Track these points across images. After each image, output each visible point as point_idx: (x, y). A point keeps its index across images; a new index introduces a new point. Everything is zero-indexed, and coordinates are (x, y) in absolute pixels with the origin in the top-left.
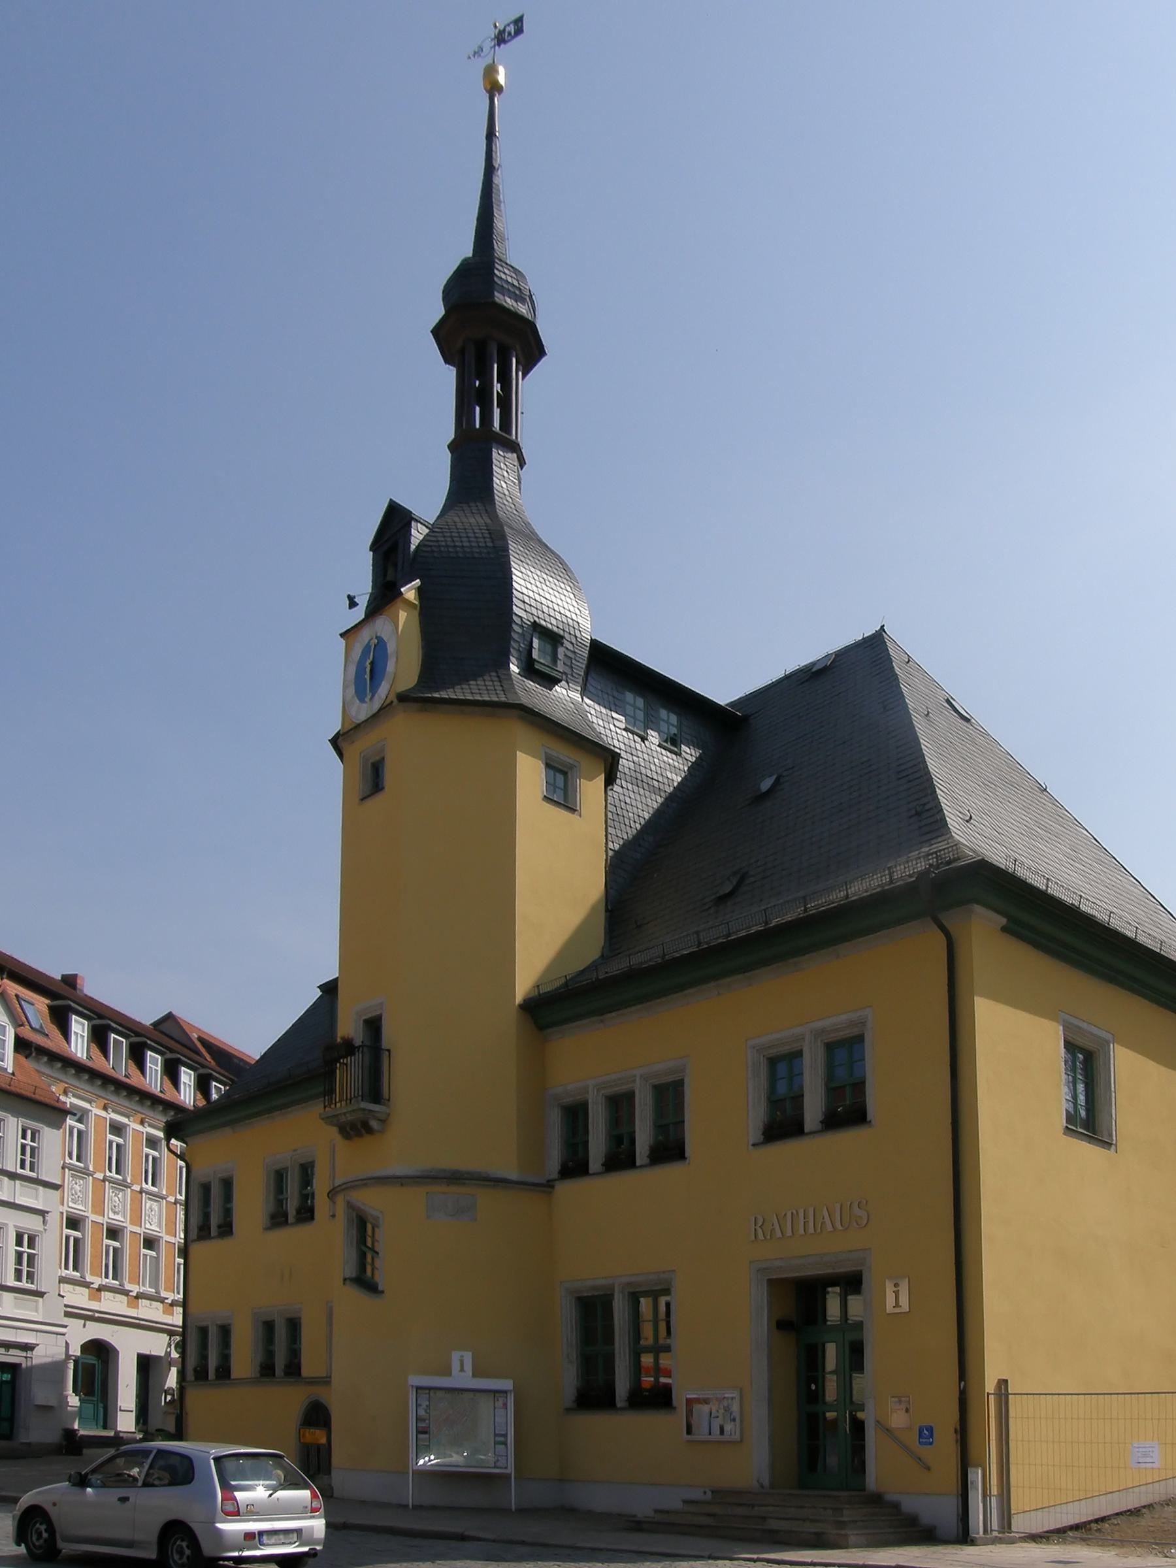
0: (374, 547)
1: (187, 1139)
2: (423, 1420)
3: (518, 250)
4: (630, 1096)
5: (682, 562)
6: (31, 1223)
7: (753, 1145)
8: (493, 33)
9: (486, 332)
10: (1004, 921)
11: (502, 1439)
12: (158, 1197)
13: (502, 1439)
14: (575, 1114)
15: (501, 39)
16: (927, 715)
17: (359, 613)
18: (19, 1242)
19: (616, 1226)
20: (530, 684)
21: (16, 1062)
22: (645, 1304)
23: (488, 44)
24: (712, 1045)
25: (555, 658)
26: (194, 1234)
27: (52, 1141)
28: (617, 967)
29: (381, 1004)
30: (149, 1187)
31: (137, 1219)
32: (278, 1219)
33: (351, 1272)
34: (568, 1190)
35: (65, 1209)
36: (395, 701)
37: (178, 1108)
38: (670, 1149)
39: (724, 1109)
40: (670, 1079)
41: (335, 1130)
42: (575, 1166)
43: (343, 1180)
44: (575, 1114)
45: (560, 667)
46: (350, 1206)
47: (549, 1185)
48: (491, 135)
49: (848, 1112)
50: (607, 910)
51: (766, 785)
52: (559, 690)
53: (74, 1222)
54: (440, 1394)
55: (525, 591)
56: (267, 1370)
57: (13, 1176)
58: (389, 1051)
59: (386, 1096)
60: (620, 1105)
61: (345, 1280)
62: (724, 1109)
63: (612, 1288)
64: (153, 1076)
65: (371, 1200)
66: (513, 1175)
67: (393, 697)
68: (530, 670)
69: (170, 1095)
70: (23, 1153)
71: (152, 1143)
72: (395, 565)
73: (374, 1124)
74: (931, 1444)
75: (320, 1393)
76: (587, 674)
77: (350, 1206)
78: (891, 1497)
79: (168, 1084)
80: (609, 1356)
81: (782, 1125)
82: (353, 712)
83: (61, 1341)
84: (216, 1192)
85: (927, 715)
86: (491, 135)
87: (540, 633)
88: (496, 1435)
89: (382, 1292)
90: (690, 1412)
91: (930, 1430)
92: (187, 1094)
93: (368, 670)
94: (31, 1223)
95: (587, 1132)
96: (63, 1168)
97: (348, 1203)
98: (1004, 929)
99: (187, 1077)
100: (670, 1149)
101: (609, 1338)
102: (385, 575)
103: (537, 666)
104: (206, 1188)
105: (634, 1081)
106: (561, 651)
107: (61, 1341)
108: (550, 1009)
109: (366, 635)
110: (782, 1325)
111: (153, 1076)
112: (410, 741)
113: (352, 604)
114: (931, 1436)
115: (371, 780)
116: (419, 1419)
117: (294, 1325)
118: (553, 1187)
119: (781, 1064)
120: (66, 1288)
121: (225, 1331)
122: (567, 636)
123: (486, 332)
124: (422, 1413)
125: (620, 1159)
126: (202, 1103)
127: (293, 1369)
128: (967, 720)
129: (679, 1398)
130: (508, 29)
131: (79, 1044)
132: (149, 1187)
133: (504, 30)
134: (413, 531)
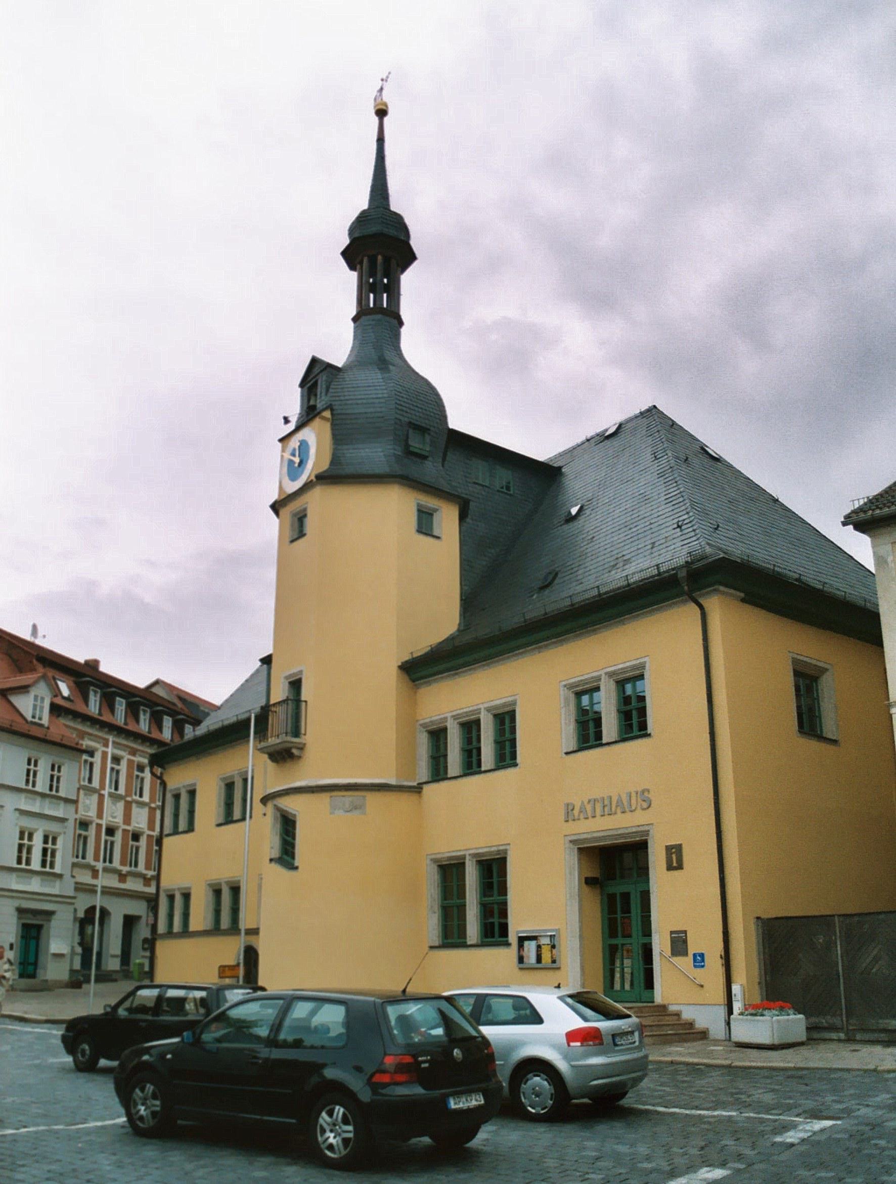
0: (302, 385)
4: (477, 722)
6: (54, 827)
9: (379, 248)
10: (742, 595)
12: (142, 804)
14: (438, 735)
16: (686, 459)
17: (291, 426)
18: (46, 841)
19: (471, 814)
21: (50, 721)
24: (536, 686)
27: (70, 777)
28: (468, 638)
29: (301, 672)
30: (137, 798)
31: (127, 819)
32: (228, 819)
33: (276, 853)
35: (78, 816)
37: (161, 743)
38: (507, 756)
39: (545, 725)
40: (507, 709)
41: (266, 756)
42: (439, 773)
44: (438, 735)
46: (277, 808)
47: (417, 789)
48: (381, 140)
49: (634, 720)
50: (461, 600)
51: (574, 511)
52: (428, 464)
53: (84, 824)
57: (43, 795)
58: (306, 702)
59: (303, 731)
61: (271, 860)
62: (545, 725)
63: (464, 857)
64: (144, 725)
65: (290, 804)
66: (393, 781)
67: (313, 477)
69: (155, 735)
70: (52, 780)
71: (141, 768)
72: (316, 395)
73: (295, 751)
74: (703, 966)
75: (252, 940)
76: (447, 447)
77: (277, 808)
78: (673, 1008)
79: (154, 726)
81: (589, 733)
82: (284, 485)
83: (71, 908)
85: (686, 459)
87: (414, 429)
89: (297, 868)
91: (702, 955)
92: (167, 734)
94: (54, 827)
95: (446, 749)
96: (79, 789)
98: (743, 600)
99: (168, 722)
101: (462, 894)
102: (309, 400)
105: (480, 713)
107: (71, 908)
108: (419, 670)
109: (294, 443)
110: (589, 882)
111: (144, 725)
112: (320, 502)
113: (286, 420)
114: (703, 961)
115: (298, 528)
117: (235, 890)
118: (422, 788)
119: (584, 690)
120: (76, 871)
121: (187, 896)
122: (432, 428)
125: (471, 764)
126: (177, 741)
127: (234, 929)
131: (94, 706)
132: (137, 798)
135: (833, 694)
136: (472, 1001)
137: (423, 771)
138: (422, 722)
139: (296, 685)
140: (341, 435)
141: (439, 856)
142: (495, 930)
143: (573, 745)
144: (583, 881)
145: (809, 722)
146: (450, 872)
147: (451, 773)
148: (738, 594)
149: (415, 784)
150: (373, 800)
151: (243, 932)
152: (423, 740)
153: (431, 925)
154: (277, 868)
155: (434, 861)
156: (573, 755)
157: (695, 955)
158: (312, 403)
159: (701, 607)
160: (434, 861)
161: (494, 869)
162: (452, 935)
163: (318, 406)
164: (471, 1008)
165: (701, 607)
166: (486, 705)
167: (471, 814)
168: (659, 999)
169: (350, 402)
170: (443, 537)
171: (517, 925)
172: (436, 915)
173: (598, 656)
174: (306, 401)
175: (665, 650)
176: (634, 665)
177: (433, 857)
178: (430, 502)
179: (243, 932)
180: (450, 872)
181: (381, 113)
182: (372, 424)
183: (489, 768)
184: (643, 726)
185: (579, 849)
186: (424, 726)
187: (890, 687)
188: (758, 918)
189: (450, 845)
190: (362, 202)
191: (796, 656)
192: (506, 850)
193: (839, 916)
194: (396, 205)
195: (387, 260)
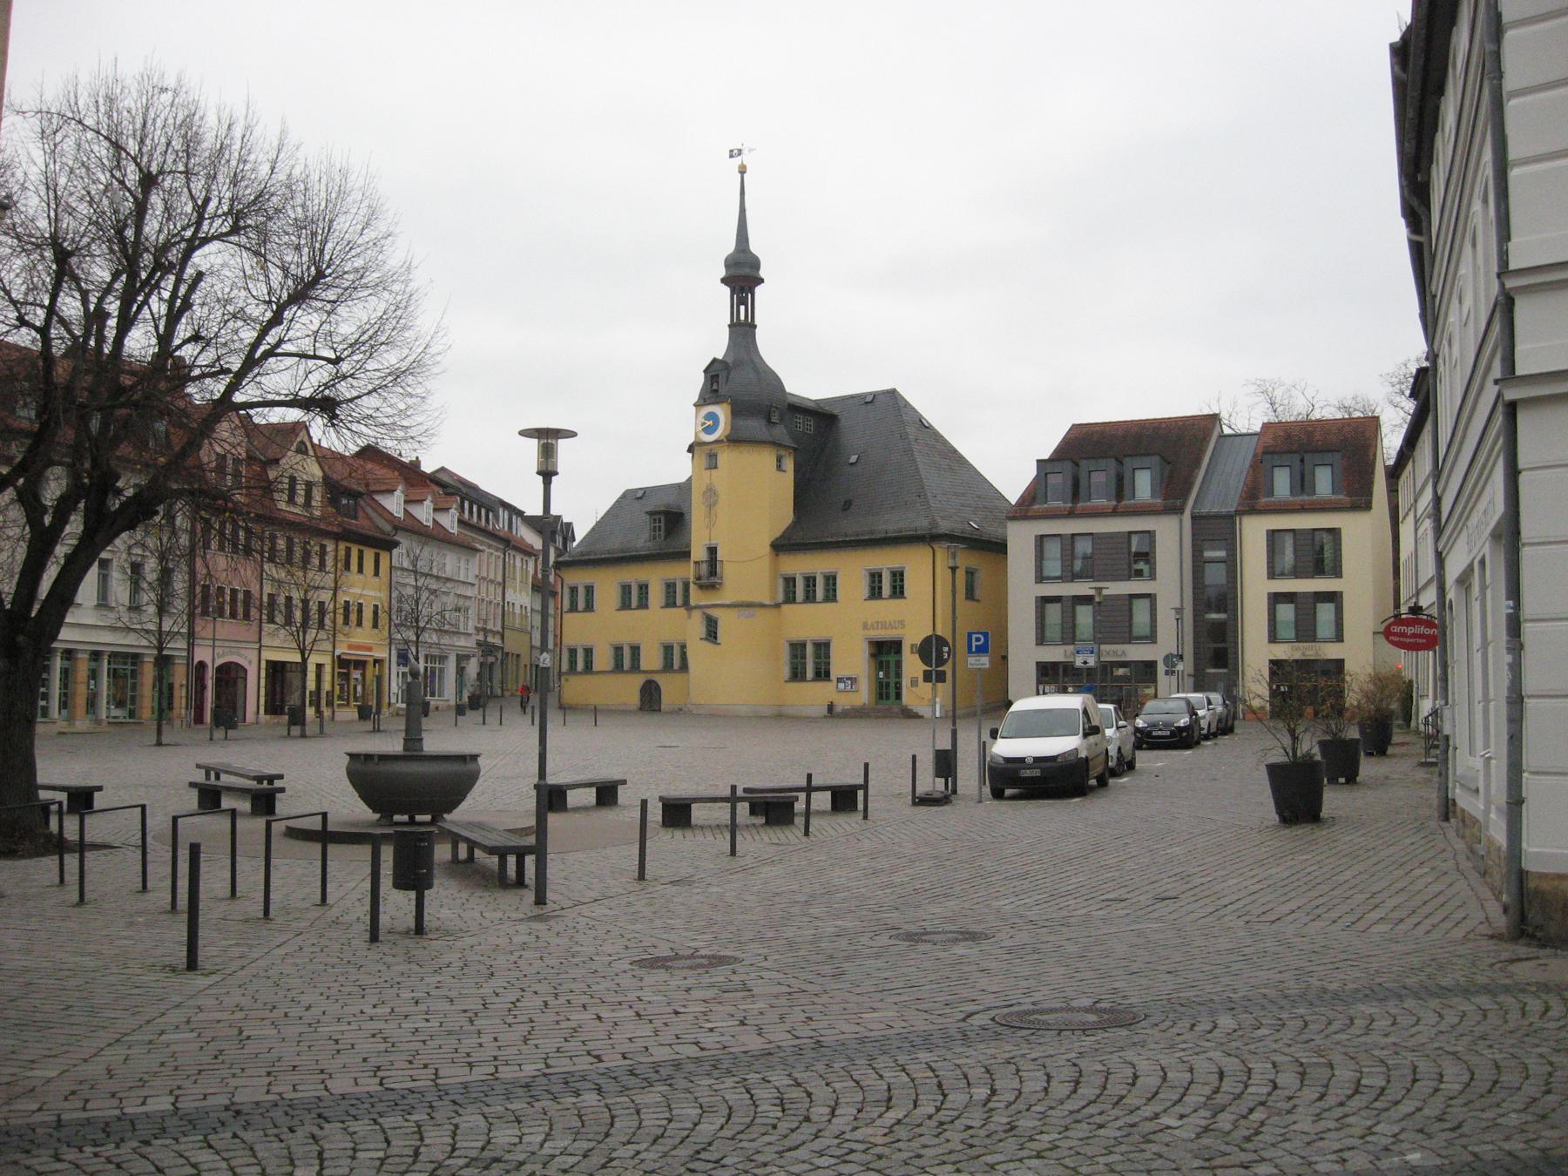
4: (880, 575)
9: (743, 277)
19: (807, 622)
24: (852, 570)
34: (786, 608)
42: (790, 598)
49: (898, 591)
56: (618, 667)
65: (714, 613)
81: (875, 593)
112: (725, 457)
123: (743, 277)
125: (810, 597)
135: (981, 579)
137: (780, 597)
140: (737, 412)
142: (823, 674)
145: (970, 595)
152: (781, 582)
153: (786, 671)
154: (706, 643)
162: (797, 675)
164: (1059, 564)
167: (807, 622)
168: (1008, 459)
171: (835, 672)
173: (885, 560)
175: (918, 566)
178: (783, 453)
180: (797, 649)
182: (741, 391)
184: (902, 592)
187: (1511, 199)
189: (798, 636)
190: (730, 247)
194: (755, 247)
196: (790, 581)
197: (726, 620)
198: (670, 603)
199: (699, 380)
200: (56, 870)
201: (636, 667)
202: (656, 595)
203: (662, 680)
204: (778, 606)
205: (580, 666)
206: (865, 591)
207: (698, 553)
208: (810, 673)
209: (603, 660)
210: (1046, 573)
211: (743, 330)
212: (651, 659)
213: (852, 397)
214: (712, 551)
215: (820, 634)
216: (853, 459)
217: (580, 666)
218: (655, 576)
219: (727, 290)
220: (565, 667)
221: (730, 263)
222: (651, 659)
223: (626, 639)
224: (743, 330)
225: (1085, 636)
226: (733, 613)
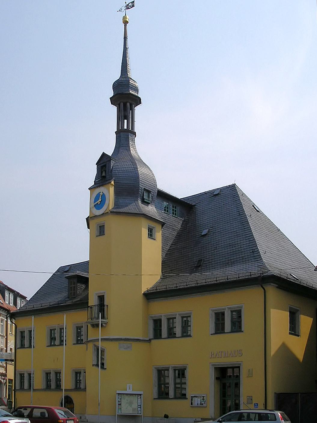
1: (16, 318)
2: (120, 402)
3: (133, 74)
4: (223, 314)
5: (179, 165)
7: (211, 334)
8: (125, 5)
9: (125, 98)
10: (277, 286)
11: (140, 406)
13: (140, 406)
15: (128, 7)
19: (170, 352)
20: (143, 205)
22: (53, 331)
23: (124, 8)
24: (200, 310)
25: (149, 197)
26: (19, 345)
34: (155, 342)
36: (109, 212)
38: (185, 334)
42: (157, 335)
43: (90, 340)
45: (150, 199)
47: (150, 340)
48: (125, 38)
49: (237, 326)
54: (125, 395)
55: (142, 180)
56: (48, 387)
60: (170, 319)
61: (93, 365)
66: (141, 339)
68: (143, 201)
77: (95, 345)
80: (169, 384)
81: (219, 329)
84: (26, 334)
86: (125, 38)
87: (146, 191)
88: (138, 405)
90: (192, 399)
93: (98, 202)
97: (94, 345)
98: (277, 287)
100: (185, 334)
103: (145, 200)
104: (22, 333)
106: (150, 195)
108: (150, 296)
110: (217, 379)
112: (114, 225)
115: (101, 231)
116: (119, 402)
118: (151, 341)
123: (125, 98)
124: (119, 400)
125: (171, 334)
128: (258, 211)
129: (188, 396)
130: (130, 4)
133: (128, 4)
134: (111, 163)
136: (247, 414)
137: (151, 336)
138: (150, 316)
139: (101, 298)
141: (157, 367)
143: (213, 332)
144: (215, 378)
146: (161, 373)
147: (163, 337)
148: (275, 285)
149: (148, 339)
150: (134, 344)
151: (64, 390)
155: (156, 368)
156: (213, 335)
157: (255, 404)
158: (104, 174)
159: (264, 289)
160: (156, 368)
161: (181, 373)
162: (163, 394)
163: (107, 177)
165: (264, 289)
166: (178, 313)
167: (170, 352)
169: (121, 177)
170: (157, 239)
172: (157, 387)
173: (226, 301)
174: (100, 174)
176: (238, 306)
177: (155, 367)
179: (64, 390)
180: (161, 373)
181: (126, 23)
183: (179, 336)
185: (215, 368)
186: (152, 317)
188: (275, 393)
189: (162, 363)
190: (117, 75)
191: (290, 306)
192: (186, 366)
193: (300, 393)
195: (131, 105)
196: (157, 323)
197: (112, 352)
198: (79, 341)
199: (92, 172)
200: (239, 370)
201: (58, 387)
202: (69, 335)
203: (74, 396)
204: (150, 340)
205: (26, 386)
206: (211, 327)
207: (93, 301)
208: (171, 394)
209: (39, 382)
210: (235, 369)
211: (125, 135)
212: (67, 382)
213: (205, 193)
214: (101, 298)
215: (178, 362)
216: (205, 232)
217: (26, 386)
218: (67, 321)
219: (114, 109)
220: (18, 387)
221: (117, 86)
222: (67, 382)
223: (51, 366)
224: (125, 135)
225: (18, 389)
226: (116, 344)
